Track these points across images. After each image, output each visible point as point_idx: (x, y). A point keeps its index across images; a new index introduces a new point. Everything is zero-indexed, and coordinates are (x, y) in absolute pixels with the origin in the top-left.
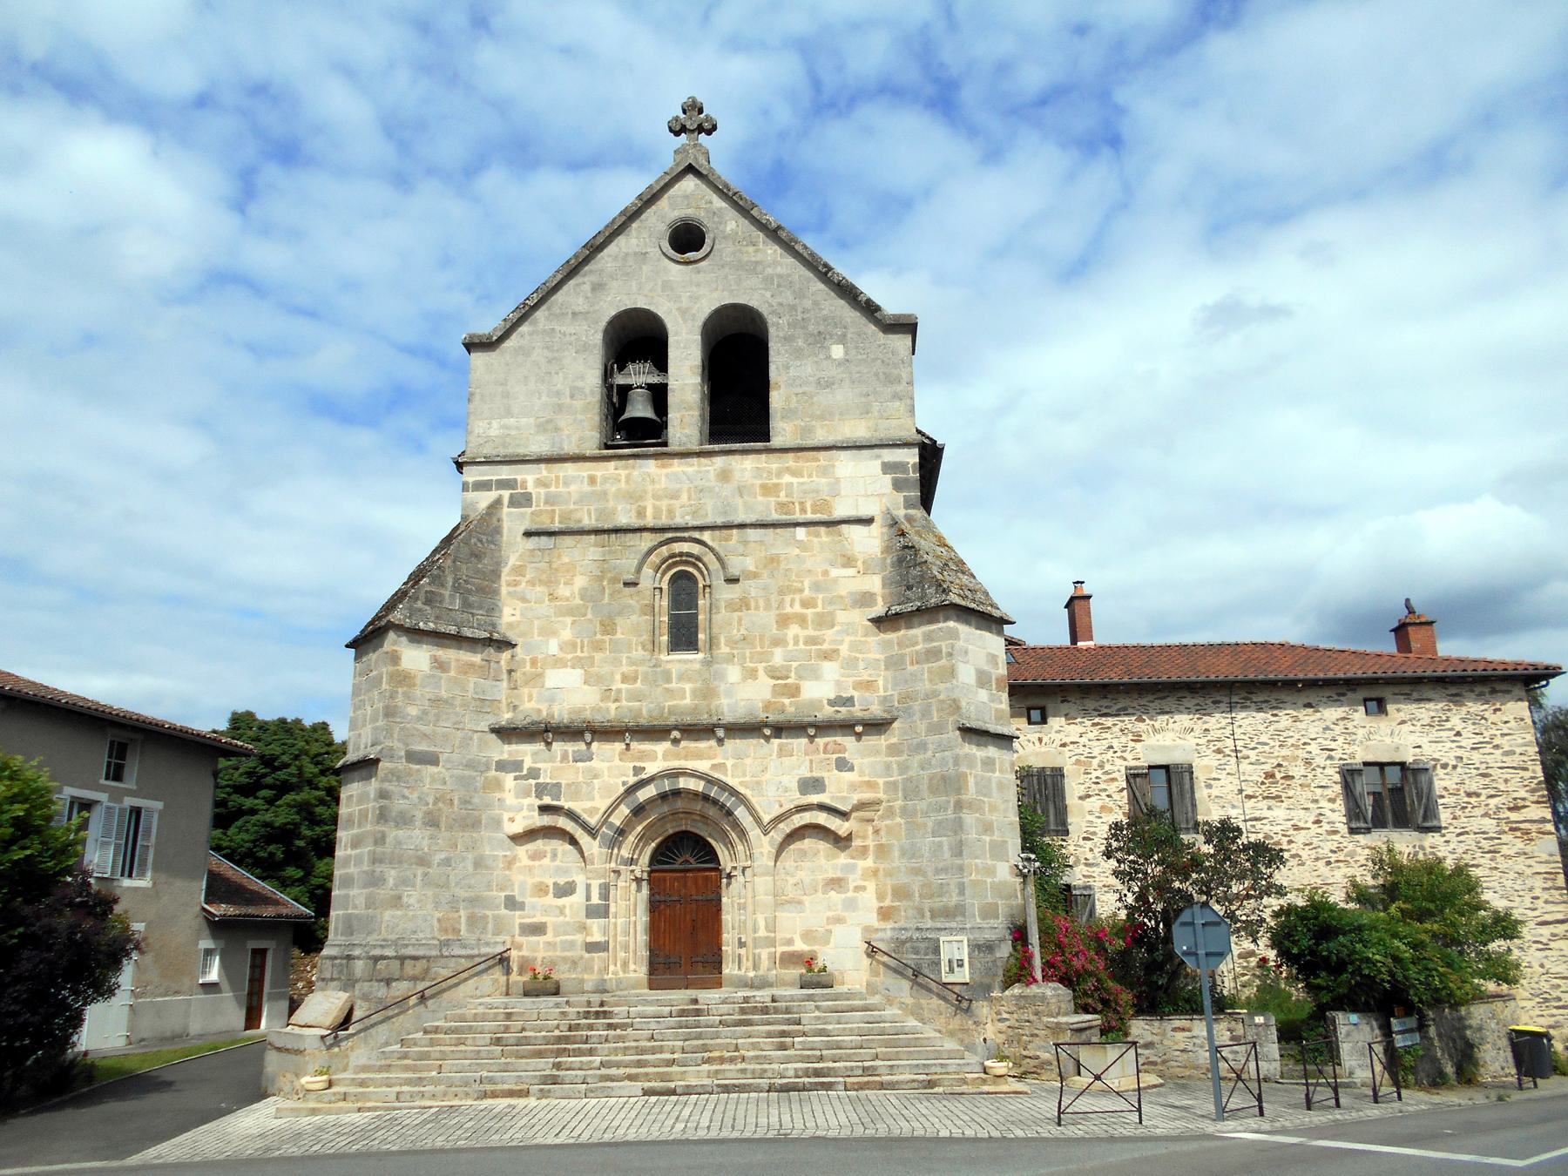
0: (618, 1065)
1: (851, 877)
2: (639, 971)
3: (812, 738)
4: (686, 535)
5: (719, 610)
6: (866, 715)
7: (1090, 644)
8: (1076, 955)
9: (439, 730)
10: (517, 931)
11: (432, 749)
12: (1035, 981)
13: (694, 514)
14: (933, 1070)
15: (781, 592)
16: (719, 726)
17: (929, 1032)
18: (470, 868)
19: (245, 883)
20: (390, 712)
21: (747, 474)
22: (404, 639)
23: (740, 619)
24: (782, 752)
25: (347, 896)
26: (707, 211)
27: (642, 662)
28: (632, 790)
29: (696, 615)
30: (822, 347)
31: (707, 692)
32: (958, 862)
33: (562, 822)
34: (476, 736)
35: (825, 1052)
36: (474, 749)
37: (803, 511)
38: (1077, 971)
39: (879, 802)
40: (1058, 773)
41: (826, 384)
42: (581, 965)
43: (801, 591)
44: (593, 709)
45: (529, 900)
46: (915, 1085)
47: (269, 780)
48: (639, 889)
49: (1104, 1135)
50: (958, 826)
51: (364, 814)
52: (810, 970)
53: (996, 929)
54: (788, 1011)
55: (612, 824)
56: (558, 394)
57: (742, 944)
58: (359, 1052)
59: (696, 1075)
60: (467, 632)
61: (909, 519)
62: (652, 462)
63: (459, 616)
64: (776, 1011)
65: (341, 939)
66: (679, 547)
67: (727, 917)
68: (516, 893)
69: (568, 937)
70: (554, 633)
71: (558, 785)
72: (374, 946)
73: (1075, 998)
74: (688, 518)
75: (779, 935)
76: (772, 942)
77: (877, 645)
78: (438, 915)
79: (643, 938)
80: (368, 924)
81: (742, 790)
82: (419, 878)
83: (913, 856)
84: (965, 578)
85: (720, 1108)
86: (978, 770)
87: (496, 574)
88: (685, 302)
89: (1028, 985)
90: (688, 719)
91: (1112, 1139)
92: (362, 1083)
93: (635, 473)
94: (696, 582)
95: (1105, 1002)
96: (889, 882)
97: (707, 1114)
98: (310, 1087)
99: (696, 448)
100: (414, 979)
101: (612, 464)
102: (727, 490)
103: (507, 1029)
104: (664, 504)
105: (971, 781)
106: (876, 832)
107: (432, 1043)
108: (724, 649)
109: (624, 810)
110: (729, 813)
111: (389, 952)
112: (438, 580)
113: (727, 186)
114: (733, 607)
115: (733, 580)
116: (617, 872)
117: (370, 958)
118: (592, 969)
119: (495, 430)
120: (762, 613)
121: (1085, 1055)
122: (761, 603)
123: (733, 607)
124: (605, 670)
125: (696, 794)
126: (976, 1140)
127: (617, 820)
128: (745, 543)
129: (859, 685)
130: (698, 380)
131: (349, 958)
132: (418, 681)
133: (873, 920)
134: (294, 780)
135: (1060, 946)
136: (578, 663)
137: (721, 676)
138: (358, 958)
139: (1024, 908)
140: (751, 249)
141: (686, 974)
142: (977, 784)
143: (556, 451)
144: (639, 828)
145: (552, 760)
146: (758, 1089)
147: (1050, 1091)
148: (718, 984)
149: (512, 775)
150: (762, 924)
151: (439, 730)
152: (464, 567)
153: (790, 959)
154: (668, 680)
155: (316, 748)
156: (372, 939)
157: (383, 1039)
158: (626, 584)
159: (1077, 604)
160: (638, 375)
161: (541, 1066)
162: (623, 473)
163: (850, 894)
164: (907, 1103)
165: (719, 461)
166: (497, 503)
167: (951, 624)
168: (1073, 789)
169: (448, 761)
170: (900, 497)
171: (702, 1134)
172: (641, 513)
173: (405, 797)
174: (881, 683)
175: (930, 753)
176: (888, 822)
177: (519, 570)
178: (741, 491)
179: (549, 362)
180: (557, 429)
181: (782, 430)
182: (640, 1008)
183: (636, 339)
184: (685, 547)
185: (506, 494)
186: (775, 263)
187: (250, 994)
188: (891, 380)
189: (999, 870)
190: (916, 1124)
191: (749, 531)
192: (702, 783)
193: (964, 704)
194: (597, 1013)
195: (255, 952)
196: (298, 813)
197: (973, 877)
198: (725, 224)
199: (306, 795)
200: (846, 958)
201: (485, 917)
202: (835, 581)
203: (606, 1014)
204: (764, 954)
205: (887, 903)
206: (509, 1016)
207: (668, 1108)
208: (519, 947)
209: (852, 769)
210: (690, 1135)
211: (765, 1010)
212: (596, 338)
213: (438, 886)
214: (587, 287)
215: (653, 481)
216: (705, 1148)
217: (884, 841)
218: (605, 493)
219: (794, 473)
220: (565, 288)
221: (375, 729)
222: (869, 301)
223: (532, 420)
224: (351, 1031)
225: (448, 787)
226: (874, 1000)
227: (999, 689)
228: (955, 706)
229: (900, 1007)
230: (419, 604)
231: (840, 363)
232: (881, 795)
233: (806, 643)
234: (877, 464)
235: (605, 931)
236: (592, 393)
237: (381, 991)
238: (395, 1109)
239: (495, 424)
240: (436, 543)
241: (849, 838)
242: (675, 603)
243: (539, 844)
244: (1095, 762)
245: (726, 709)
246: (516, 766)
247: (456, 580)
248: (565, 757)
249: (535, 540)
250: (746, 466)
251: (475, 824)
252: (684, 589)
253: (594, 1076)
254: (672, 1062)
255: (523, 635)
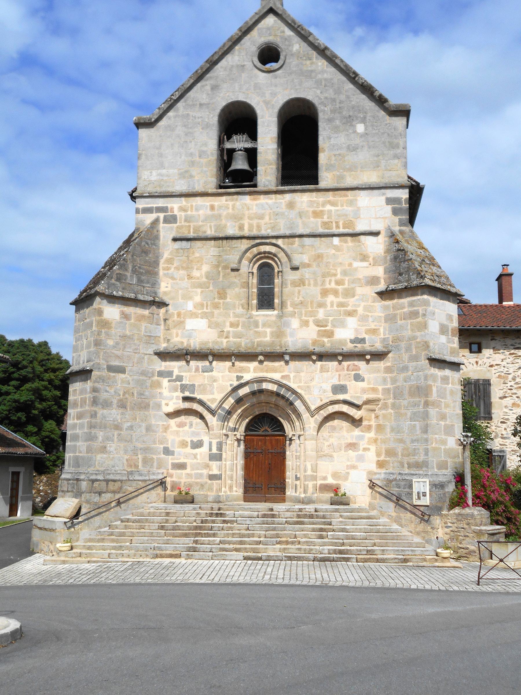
0: (229, 543)
1: (361, 443)
2: (238, 491)
3: (340, 362)
4: (268, 241)
5: (285, 285)
6: (373, 349)
7: (511, 303)
8: (493, 492)
9: (125, 353)
10: (170, 467)
11: (121, 364)
12: (468, 506)
13: (273, 228)
14: (407, 553)
15: (324, 276)
16: (286, 353)
17: (405, 532)
18: (144, 431)
19: (5, 434)
20: (97, 343)
21: (304, 205)
22: (105, 301)
23: (299, 292)
24: (322, 370)
25: (75, 446)
26: (282, 37)
27: (242, 316)
28: (235, 389)
29: (273, 288)
30: (351, 125)
31: (279, 334)
32: (425, 436)
33: (196, 406)
34: (146, 357)
35: (345, 541)
36: (145, 364)
37: (338, 227)
38: (493, 501)
39: (378, 400)
40: (487, 383)
41: (353, 149)
42: (206, 486)
43: (335, 275)
44: (213, 342)
45: (177, 450)
46: (397, 561)
47: (16, 375)
48: (239, 445)
49: (503, 591)
50: (426, 416)
51: (83, 401)
52: (336, 495)
53: (447, 475)
54: (324, 517)
55: (224, 408)
56: (191, 154)
57: (297, 479)
58: (84, 532)
59: (274, 550)
60: (141, 297)
61: (402, 232)
62: (247, 197)
63: (136, 288)
64: (318, 517)
65: (72, 469)
66: (263, 248)
67: (290, 463)
68: (169, 446)
69: (199, 471)
70: (191, 298)
71: (193, 385)
72: (92, 474)
73: (491, 516)
74: (269, 231)
75: (319, 474)
76: (314, 478)
77: (380, 307)
78: (126, 457)
79: (241, 472)
80: (89, 462)
81: (299, 391)
82: (116, 437)
83: (398, 432)
84: (434, 269)
85: (288, 569)
86: (439, 383)
87: (156, 263)
88: (268, 96)
89: (464, 507)
90: (268, 349)
91: (508, 593)
92: (89, 548)
93: (238, 203)
94: (273, 269)
95: (509, 519)
96: (384, 446)
97: (281, 571)
98: (60, 549)
99: (274, 188)
100: (114, 492)
101: (224, 198)
102: (292, 214)
103: (167, 521)
104: (255, 222)
105: (434, 389)
106: (377, 417)
107: (126, 527)
108: (290, 309)
109: (231, 401)
110: (291, 404)
111: (100, 477)
112: (123, 267)
113: (294, 21)
114: (295, 284)
115: (295, 268)
116: (227, 436)
117: (90, 480)
118: (212, 489)
119: (154, 177)
120: (312, 287)
121: (495, 548)
122: (312, 282)
123: (295, 284)
124: (220, 320)
125: (272, 392)
126: (431, 591)
127: (227, 406)
128: (303, 246)
129: (368, 331)
130: (275, 146)
131: (78, 480)
132: (113, 325)
133: (373, 467)
134: (31, 375)
135: (484, 486)
136: (205, 315)
137: (287, 324)
138: (83, 480)
139: (463, 463)
140: (308, 62)
141: (265, 494)
142: (438, 391)
143: (190, 190)
144: (239, 411)
145: (190, 371)
146: (307, 559)
147: (474, 567)
148: (283, 500)
149: (167, 379)
150: (309, 467)
151: (125, 353)
152: (138, 259)
153: (325, 488)
154: (257, 326)
155: (41, 357)
156: (91, 470)
157: (97, 525)
158: (233, 270)
159: (504, 280)
160: (239, 143)
161: (187, 542)
162: (231, 203)
163: (361, 452)
164: (392, 570)
165: (288, 197)
166: (157, 220)
167: (425, 297)
168: (496, 392)
169: (130, 371)
170: (396, 219)
171: (280, 581)
172: (241, 228)
173: (107, 391)
174: (382, 330)
175: (410, 373)
176: (384, 412)
177: (170, 261)
178: (300, 215)
179: (186, 135)
180: (191, 176)
181: (326, 178)
182: (240, 512)
183: (238, 121)
184: (267, 248)
185: (162, 215)
186: (323, 72)
187: (11, 497)
188: (393, 146)
189: (449, 442)
190: (398, 582)
191: (306, 239)
192: (276, 386)
193: (431, 344)
194: (217, 514)
195: (14, 473)
196: (33, 395)
197: (434, 445)
198: (293, 47)
199: (36, 384)
200: (357, 490)
201: (152, 459)
202: (356, 269)
203: (221, 515)
204: (310, 484)
205: (382, 458)
206: (168, 514)
207: (259, 567)
208: (171, 476)
209: (363, 380)
210: (273, 581)
211: (311, 516)
212: (214, 120)
213: (126, 441)
214: (208, 88)
215: (248, 209)
216: (284, 589)
217: (381, 422)
218: (220, 216)
219: (333, 204)
220: (195, 88)
221: (89, 352)
222: (380, 96)
223: (176, 171)
224: (80, 519)
225: (131, 386)
226: (374, 513)
227: (453, 335)
228: (426, 345)
229: (388, 517)
230: (113, 281)
231: (362, 136)
232: (380, 396)
233: (338, 306)
234: (383, 198)
235: (220, 468)
236: (212, 154)
237: (96, 498)
238: (108, 562)
239: (154, 173)
240: (120, 244)
241: (361, 420)
242: (261, 281)
243: (183, 418)
244: (510, 377)
245: (290, 344)
246: (168, 374)
247: (134, 267)
248: (197, 370)
249: (179, 243)
250: (304, 200)
251: (146, 407)
252: (266, 273)
253: (216, 548)
254: (259, 543)
255: (173, 298)
